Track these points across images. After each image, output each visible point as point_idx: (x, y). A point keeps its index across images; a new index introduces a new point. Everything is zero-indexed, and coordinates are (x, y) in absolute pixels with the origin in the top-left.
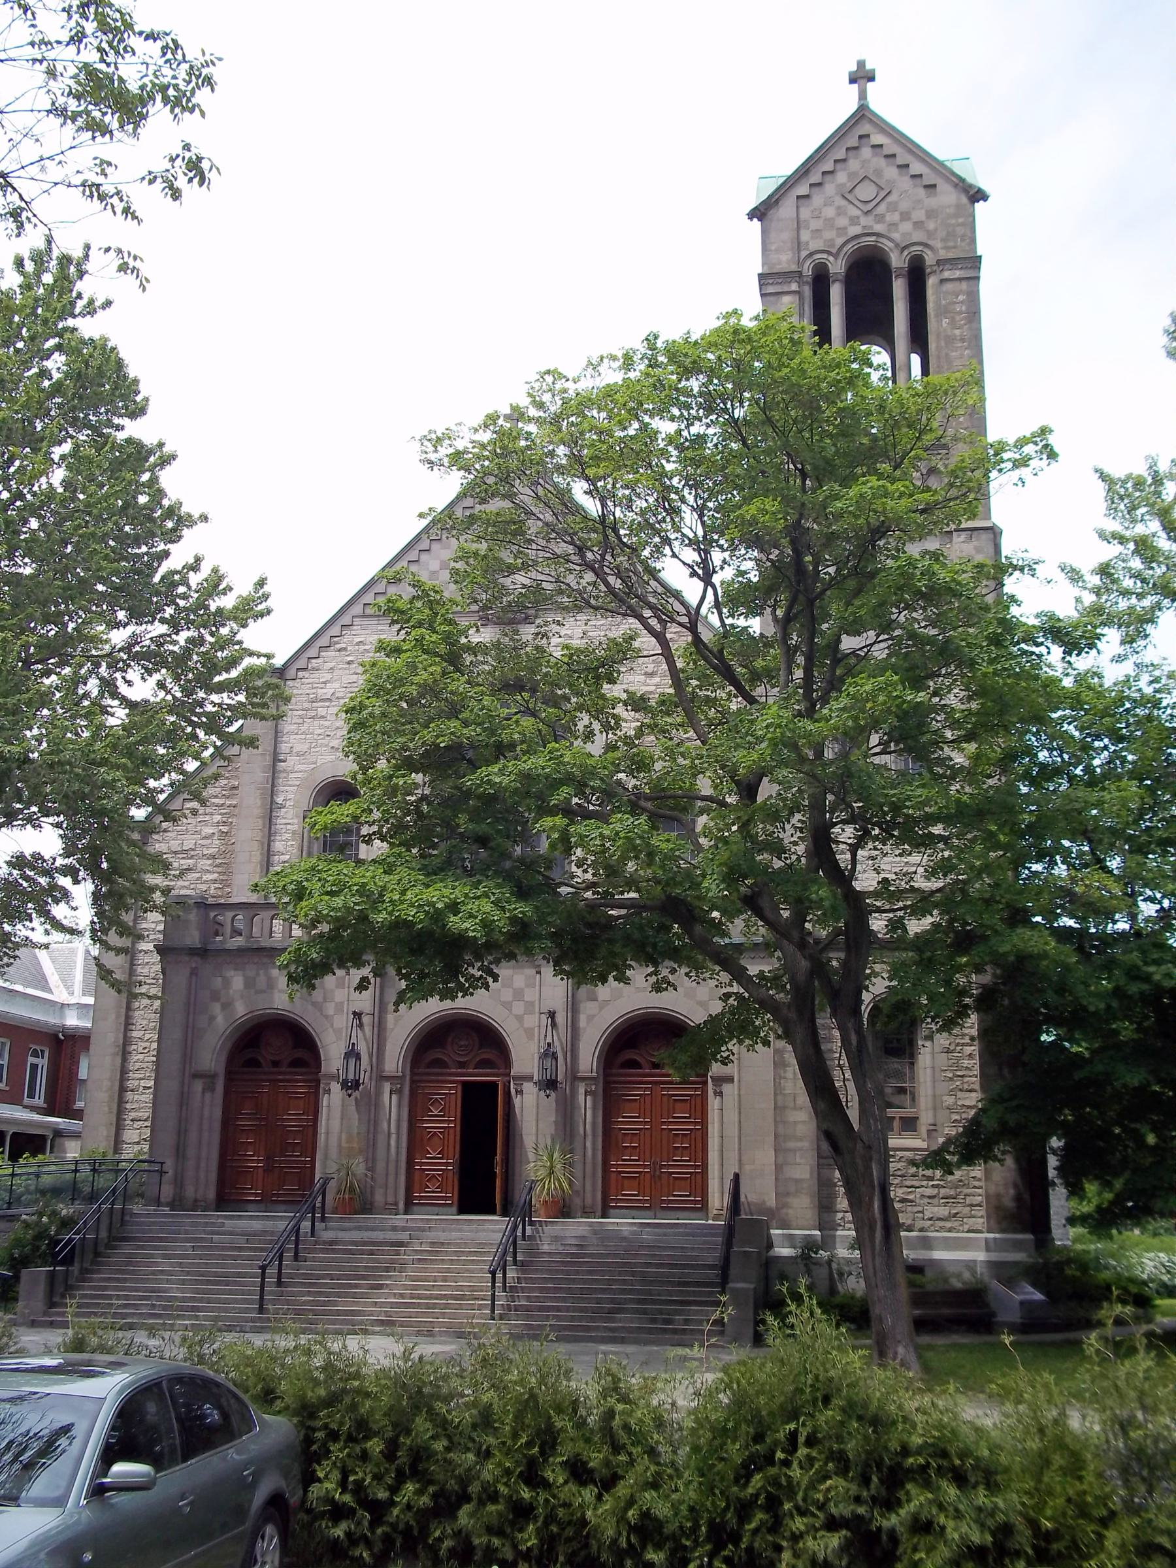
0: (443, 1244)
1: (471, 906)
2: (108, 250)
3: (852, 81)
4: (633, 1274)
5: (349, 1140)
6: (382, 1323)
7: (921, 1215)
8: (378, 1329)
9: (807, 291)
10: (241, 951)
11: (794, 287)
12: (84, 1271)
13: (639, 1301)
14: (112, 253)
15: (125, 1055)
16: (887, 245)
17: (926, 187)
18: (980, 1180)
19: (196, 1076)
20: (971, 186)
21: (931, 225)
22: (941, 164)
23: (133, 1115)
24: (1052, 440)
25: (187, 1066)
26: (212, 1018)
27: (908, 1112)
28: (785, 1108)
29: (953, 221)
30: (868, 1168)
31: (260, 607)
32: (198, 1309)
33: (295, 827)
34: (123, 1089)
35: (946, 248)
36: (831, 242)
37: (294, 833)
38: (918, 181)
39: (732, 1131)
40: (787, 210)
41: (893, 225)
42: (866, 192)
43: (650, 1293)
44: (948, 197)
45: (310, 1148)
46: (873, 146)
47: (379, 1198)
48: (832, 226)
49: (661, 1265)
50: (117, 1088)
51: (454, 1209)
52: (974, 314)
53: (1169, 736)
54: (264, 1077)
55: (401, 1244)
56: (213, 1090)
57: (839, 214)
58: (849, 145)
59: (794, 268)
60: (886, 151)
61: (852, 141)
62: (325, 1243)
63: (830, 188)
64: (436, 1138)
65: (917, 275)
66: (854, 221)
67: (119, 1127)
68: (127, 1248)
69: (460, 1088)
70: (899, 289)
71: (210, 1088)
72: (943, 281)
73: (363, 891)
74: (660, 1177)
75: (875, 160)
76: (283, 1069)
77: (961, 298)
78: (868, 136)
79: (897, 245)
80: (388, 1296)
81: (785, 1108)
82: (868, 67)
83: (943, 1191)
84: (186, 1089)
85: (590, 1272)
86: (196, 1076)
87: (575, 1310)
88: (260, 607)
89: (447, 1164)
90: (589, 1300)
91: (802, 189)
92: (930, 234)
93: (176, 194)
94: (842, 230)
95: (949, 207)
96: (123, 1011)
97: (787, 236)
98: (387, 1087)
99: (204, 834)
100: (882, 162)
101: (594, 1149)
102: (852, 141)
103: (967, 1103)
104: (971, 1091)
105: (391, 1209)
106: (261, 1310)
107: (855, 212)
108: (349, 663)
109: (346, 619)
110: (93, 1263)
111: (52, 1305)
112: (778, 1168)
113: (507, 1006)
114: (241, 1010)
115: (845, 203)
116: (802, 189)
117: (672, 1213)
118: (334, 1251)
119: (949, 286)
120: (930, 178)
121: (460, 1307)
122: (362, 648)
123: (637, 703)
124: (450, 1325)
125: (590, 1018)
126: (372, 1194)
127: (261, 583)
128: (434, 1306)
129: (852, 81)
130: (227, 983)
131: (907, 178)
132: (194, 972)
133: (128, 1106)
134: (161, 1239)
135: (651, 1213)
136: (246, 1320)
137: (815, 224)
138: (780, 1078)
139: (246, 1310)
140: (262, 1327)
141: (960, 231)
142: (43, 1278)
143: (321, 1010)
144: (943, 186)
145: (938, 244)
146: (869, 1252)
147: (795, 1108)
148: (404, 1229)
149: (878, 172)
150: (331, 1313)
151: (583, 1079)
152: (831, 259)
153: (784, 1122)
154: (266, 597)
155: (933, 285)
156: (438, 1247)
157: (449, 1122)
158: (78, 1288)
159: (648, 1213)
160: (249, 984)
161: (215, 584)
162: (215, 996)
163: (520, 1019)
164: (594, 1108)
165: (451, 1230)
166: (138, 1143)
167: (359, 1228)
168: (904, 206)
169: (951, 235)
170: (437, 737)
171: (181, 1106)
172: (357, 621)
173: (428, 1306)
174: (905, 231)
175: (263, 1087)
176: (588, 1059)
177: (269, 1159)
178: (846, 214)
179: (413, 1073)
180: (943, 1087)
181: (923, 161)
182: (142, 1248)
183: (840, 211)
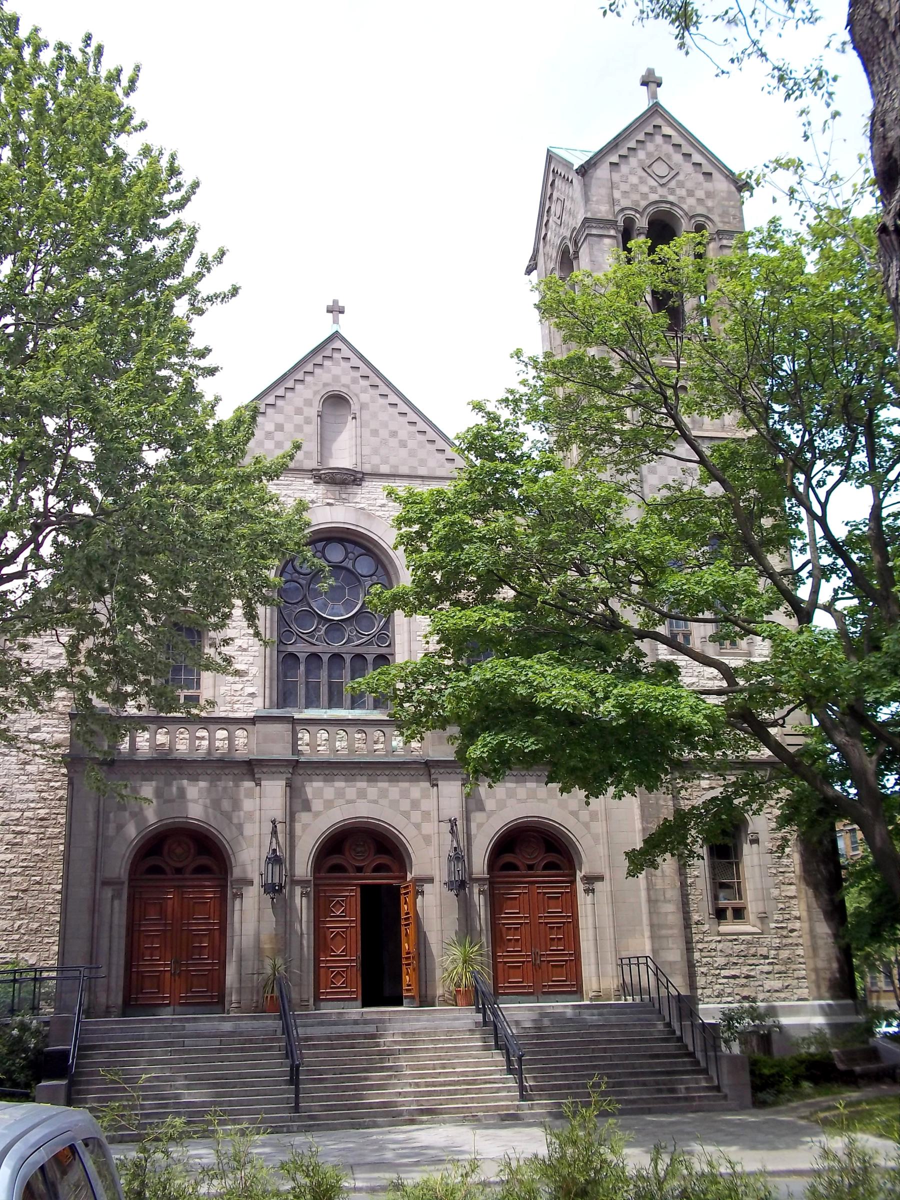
0: (414, 1034)
6: (422, 1112)
7: (761, 988)
8: (425, 1118)
17: (704, 173)
18: (803, 957)
19: (106, 883)
21: (710, 203)
25: (98, 874)
26: (120, 827)
27: (736, 903)
28: (657, 901)
29: (726, 203)
36: (637, 203)
38: (698, 168)
39: (607, 922)
40: (602, 172)
41: (681, 198)
42: (660, 169)
43: (633, 1066)
44: (721, 185)
46: (664, 136)
51: (359, 1002)
54: (189, 883)
55: (373, 1036)
58: (647, 131)
59: (611, 217)
63: (633, 161)
64: (339, 937)
66: (653, 190)
69: (359, 889)
71: (116, 896)
72: (722, 247)
76: (187, 876)
78: (660, 127)
81: (657, 901)
83: (776, 967)
84: (97, 896)
86: (106, 883)
89: (351, 961)
91: (614, 159)
92: (710, 210)
94: (644, 196)
95: (722, 192)
97: (604, 191)
99: (51, 654)
100: (670, 149)
103: (789, 894)
104: (791, 884)
106: (296, 1109)
113: (406, 815)
114: (151, 816)
115: (645, 174)
116: (614, 159)
117: (552, 997)
120: (707, 168)
125: (480, 826)
128: (455, 1092)
129: (644, 83)
131: (690, 165)
137: (624, 187)
138: (652, 875)
140: (310, 1126)
141: (732, 211)
143: (230, 819)
144: (716, 175)
145: (716, 218)
149: (669, 156)
151: (477, 880)
152: (638, 215)
153: (658, 913)
155: (713, 249)
159: (531, 997)
160: (159, 793)
163: (418, 826)
168: (689, 185)
178: (646, 183)
180: (771, 881)
181: (702, 154)
182: (115, 1055)
183: (642, 181)
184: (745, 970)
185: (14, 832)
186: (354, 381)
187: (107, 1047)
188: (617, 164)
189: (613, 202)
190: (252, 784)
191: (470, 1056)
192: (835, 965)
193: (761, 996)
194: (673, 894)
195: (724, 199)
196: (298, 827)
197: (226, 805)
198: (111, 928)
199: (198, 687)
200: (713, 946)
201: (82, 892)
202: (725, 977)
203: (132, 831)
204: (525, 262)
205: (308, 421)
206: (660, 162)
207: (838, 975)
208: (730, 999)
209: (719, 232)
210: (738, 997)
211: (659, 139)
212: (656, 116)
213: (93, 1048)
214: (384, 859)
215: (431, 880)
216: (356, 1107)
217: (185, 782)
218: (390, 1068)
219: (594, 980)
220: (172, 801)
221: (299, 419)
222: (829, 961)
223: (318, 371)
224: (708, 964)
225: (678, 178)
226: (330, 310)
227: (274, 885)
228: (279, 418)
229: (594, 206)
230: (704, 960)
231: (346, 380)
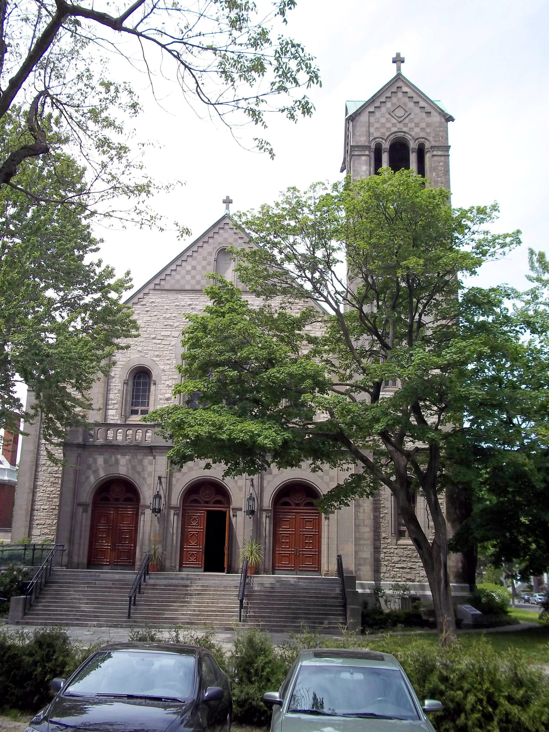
1: (265, 433)
2: (256, 139)
3: (394, 62)
4: (300, 601)
5: (155, 537)
6: (188, 623)
9: (372, 155)
10: (102, 446)
11: (367, 153)
12: (37, 598)
13: (305, 614)
14: (257, 141)
15: (34, 493)
16: (408, 137)
19: (80, 505)
20: (447, 114)
21: (428, 130)
22: (432, 102)
23: (37, 522)
24: (521, 237)
26: (88, 478)
28: (359, 525)
30: (439, 556)
31: (128, 285)
32: (97, 616)
33: (120, 388)
34: (33, 510)
35: (435, 141)
36: (384, 134)
37: (119, 390)
38: (423, 110)
39: (334, 535)
40: (364, 118)
42: (400, 112)
43: (309, 610)
44: (436, 118)
45: (134, 540)
47: (168, 564)
48: (384, 127)
49: (311, 597)
50: (30, 509)
51: (202, 569)
52: (447, 172)
53: (543, 367)
55: (187, 586)
56: (87, 512)
57: (387, 122)
59: (367, 144)
60: (409, 95)
61: (394, 89)
62: (151, 585)
63: (383, 110)
65: (421, 152)
66: (394, 125)
67: (30, 528)
68: (55, 587)
70: (413, 158)
71: (85, 511)
72: (433, 156)
73: (214, 425)
74: (299, 556)
75: (404, 98)
77: (441, 164)
79: (413, 138)
80: (187, 611)
81: (359, 525)
82: (402, 56)
85: (280, 600)
87: (277, 617)
88: (128, 285)
89: (199, 548)
90: (283, 613)
91: (371, 109)
92: (428, 134)
93: (292, 117)
96: (34, 472)
97: (364, 129)
98: (172, 512)
100: (407, 100)
101: (269, 543)
102: (394, 89)
105: (172, 569)
106: (129, 617)
107: (394, 121)
108: (147, 311)
109: (146, 291)
110: (40, 594)
111: (25, 614)
112: (356, 553)
114: (102, 474)
115: (390, 117)
116: (371, 109)
117: (304, 573)
118: (156, 589)
119: (436, 158)
120: (428, 109)
121: (223, 616)
122: (154, 304)
123: (312, 340)
124: (221, 625)
125: (269, 482)
126: (165, 561)
127: (128, 273)
128: (211, 615)
129: (394, 62)
130: (95, 461)
131: (418, 108)
132: (79, 455)
133: (35, 518)
134: (70, 583)
135: (295, 572)
136: (122, 622)
137: (377, 125)
139: (121, 617)
142: (22, 602)
144: (434, 113)
145: (431, 139)
146: (437, 594)
147: (364, 526)
148: (188, 579)
149: (405, 104)
150: (163, 618)
154: (131, 280)
156: (205, 588)
157: (200, 529)
158: (36, 606)
160: (106, 462)
161: (109, 273)
162: (89, 467)
164: (270, 524)
165: (209, 580)
166: (39, 536)
167: (166, 578)
168: (416, 120)
169: (437, 135)
170: (249, 354)
171: (72, 519)
172: (151, 292)
173: (208, 615)
174: (416, 132)
175: (111, 511)
176: (267, 502)
177: (113, 545)
179: (183, 506)
181: (425, 100)
182: (62, 587)
183: (388, 120)
184: (409, 564)
185: (54, 477)
186: (235, 240)
187: (60, 583)
188: (373, 112)
189: (369, 134)
190: (152, 458)
191: (229, 599)
192: (460, 565)
193: (417, 579)
194: (369, 522)
195: (437, 127)
196: (174, 480)
197: (139, 468)
198: (81, 526)
199: (148, 406)
200: (392, 551)
201: (68, 509)
202: (397, 568)
203: (92, 479)
204: (340, 165)
205: (209, 264)
206: (400, 108)
207: (461, 570)
208: (399, 580)
209: (432, 147)
210: (404, 579)
211: (400, 95)
212: (399, 81)
213: (53, 582)
214: (219, 498)
215: (240, 509)
216: (159, 618)
217: (119, 456)
218: (186, 602)
219: (326, 565)
220: (112, 465)
221: (204, 263)
222: (457, 562)
223: (216, 236)
224: (388, 560)
225: (411, 117)
226: (224, 202)
227: (155, 509)
228: (194, 263)
229: (358, 139)
230: (386, 558)
231: (231, 240)
